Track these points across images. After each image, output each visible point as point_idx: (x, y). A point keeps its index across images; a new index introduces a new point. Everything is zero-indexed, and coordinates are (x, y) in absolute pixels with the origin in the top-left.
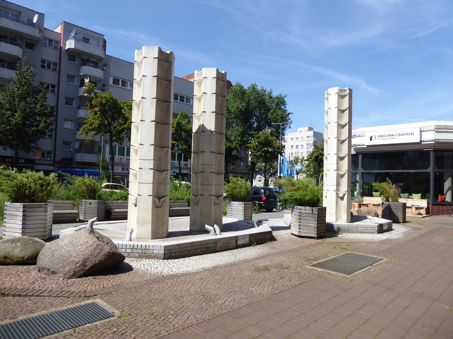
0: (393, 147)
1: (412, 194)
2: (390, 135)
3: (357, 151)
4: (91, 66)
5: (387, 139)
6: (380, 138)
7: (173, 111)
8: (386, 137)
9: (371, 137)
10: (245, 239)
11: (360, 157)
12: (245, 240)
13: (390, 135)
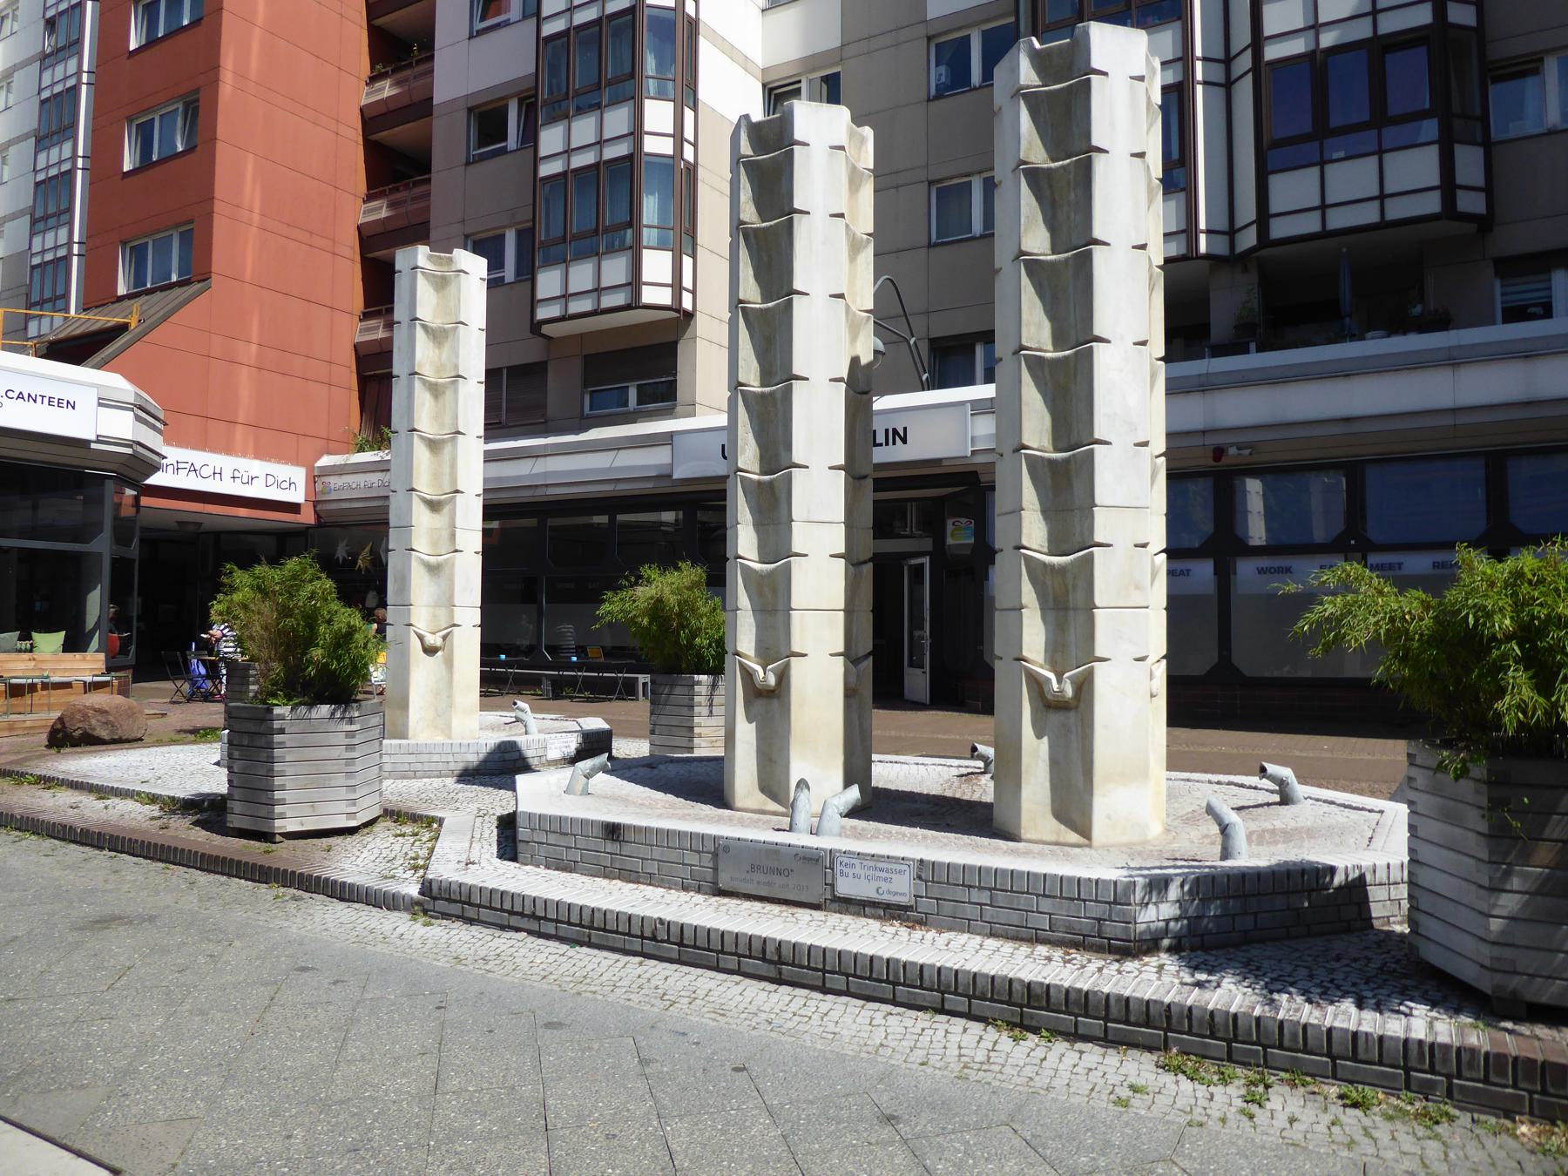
1: (1045, 739)
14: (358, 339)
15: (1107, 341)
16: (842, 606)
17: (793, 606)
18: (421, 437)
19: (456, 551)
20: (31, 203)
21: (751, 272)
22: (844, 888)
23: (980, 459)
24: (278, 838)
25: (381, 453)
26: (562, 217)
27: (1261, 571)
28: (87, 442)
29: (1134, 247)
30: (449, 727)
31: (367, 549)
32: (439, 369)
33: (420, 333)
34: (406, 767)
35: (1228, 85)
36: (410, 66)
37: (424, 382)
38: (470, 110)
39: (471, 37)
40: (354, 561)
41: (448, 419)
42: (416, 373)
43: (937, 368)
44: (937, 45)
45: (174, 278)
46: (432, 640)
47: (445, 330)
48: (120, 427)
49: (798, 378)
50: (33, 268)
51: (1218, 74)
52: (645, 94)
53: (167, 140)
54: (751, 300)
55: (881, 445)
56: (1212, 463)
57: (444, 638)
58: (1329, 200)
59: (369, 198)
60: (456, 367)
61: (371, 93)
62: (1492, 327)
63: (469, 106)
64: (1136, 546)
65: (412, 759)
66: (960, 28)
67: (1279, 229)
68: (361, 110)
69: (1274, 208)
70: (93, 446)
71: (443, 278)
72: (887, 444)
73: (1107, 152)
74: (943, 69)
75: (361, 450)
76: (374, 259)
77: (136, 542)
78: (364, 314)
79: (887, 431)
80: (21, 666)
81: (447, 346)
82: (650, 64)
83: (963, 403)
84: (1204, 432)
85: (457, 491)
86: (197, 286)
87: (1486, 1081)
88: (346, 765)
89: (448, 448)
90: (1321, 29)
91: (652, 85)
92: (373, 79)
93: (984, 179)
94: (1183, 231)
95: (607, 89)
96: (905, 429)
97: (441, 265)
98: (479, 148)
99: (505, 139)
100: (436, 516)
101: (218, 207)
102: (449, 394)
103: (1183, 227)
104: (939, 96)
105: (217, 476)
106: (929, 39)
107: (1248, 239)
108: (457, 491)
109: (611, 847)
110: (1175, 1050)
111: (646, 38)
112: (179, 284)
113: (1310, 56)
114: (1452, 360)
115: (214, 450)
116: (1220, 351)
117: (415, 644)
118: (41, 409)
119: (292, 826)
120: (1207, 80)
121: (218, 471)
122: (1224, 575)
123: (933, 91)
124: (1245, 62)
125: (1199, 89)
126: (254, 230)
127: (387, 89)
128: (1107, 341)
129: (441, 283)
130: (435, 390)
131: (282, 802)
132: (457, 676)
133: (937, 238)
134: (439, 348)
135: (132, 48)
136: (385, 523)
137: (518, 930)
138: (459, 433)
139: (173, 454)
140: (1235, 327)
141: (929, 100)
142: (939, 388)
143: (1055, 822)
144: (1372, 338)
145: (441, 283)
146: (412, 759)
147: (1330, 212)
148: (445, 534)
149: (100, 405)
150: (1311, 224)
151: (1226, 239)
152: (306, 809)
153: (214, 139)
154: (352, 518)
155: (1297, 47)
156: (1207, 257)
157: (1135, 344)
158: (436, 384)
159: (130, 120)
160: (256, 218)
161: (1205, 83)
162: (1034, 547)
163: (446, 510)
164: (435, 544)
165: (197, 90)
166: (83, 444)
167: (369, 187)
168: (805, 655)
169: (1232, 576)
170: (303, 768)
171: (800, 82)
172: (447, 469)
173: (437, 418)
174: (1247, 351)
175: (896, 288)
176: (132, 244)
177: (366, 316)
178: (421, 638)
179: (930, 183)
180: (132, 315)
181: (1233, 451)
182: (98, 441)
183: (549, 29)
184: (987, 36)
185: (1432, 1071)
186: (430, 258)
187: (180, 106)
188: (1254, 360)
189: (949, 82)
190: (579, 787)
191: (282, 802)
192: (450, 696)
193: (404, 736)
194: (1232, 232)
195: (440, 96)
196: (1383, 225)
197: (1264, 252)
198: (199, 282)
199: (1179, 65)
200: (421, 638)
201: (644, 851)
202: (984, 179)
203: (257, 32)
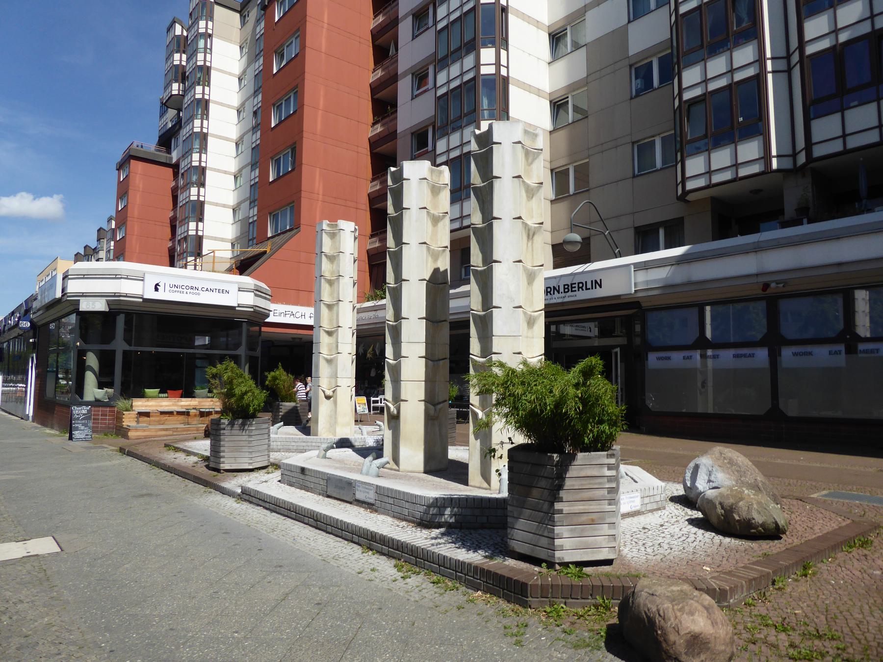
0: (198, 309)
1: (479, 440)
2: (192, 288)
3: (112, 307)
4: (630, 264)
5: (187, 293)
6: (173, 289)
7: (549, 270)
8: (185, 290)
9: (157, 285)
10: (633, 502)
11: (121, 320)
12: (633, 504)
13: (192, 288)
14: (369, 247)
15: (500, 262)
16: (424, 379)
17: (402, 379)
18: (324, 304)
19: (339, 353)
20: (249, 195)
21: (392, 235)
22: (360, 496)
23: (640, 295)
24: (222, 471)
25: (375, 302)
26: (459, 181)
27: (795, 354)
28: (234, 307)
29: (514, 219)
30: (335, 432)
31: (372, 347)
32: (332, 273)
33: (324, 258)
34: (302, 448)
35: (789, 71)
36: (388, 116)
37: (326, 279)
38: (412, 134)
39: (412, 99)
40: (366, 355)
41: (335, 295)
42: (322, 276)
43: (640, 243)
44: (636, 68)
45: (288, 228)
46: (329, 393)
47: (334, 256)
48: (248, 300)
49: (405, 280)
50: (250, 223)
51: (782, 65)
52: (481, 118)
53: (285, 166)
54: (392, 247)
55: (589, 289)
56: (760, 292)
57: (334, 392)
58: (847, 132)
59: (373, 180)
60: (339, 271)
61: (374, 130)
62: (800, 227)
63: (412, 131)
64: (514, 353)
65: (304, 444)
66: (646, 58)
67: (819, 151)
68: (369, 139)
69: (815, 139)
70: (237, 309)
71: (333, 233)
72: (592, 288)
73: (500, 178)
74: (639, 81)
75: (368, 301)
76: (377, 209)
77: (259, 349)
78: (371, 235)
79: (592, 281)
80: (208, 404)
81: (335, 263)
82: (485, 103)
83: (628, 265)
84: (757, 275)
85: (339, 327)
86: (295, 231)
87: (473, 577)
88: (249, 443)
89: (335, 308)
90: (840, 32)
91: (486, 113)
92: (374, 124)
93: (662, 138)
94: (762, 158)
95: (465, 118)
96: (601, 280)
97: (333, 228)
98: (418, 150)
99: (427, 146)
100: (330, 338)
101: (303, 194)
102: (336, 284)
103: (762, 155)
104: (637, 95)
105: (303, 317)
106: (631, 66)
107: (802, 159)
108: (339, 327)
109: (302, 477)
110: (402, 560)
111: (481, 90)
112: (290, 230)
113: (833, 49)
114: (757, 248)
115: (302, 305)
116: (785, 225)
117: (322, 395)
118: (216, 294)
119: (227, 467)
120: (774, 70)
121: (303, 314)
122: (774, 357)
123: (634, 93)
124: (796, 58)
125: (770, 77)
126: (320, 202)
127: (379, 129)
128: (500, 262)
129: (333, 235)
130: (330, 283)
131: (223, 457)
132: (339, 409)
133: (638, 172)
134: (332, 264)
135: (272, 126)
136: (312, 343)
137: (261, 506)
138: (340, 301)
139: (272, 306)
140: (795, 210)
141: (631, 98)
142: (642, 253)
143: (481, 478)
144: (878, 211)
145: (333, 235)
146: (304, 444)
147: (848, 139)
148: (334, 346)
149: (239, 290)
150: (837, 147)
151: (791, 159)
152: (232, 460)
153: (301, 164)
154: (366, 334)
155: (825, 44)
156: (778, 171)
157: (514, 262)
158: (330, 280)
159: (272, 158)
160: (321, 196)
161: (773, 72)
162: (475, 354)
163: (335, 335)
164: (330, 350)
165: (295, 143)
166: (233, 308)
167: (373, 175)
168: (407, 401)
169: (778, 358)
170: (231, 444)
171: (568, 97)
172: (335, 317)
173: (331, 294)
174: (802, 224)
175: (596, 208)
176: (274, 213)
177: (372, 236)
178: (324, 392)
179: (633, 143)
180: (267, 247)
181: (773, 285)
182: (239, 306)
183: (440, 92)
184: (661, 60)
185: (461, 573)
186: (328, 225)
187: (290, 150)
188: (807, 229)
189: (643, 87)
190: (321, 455)
191: (223, 457)
192: (336, 418)
193: (316, 435)
194: (794, 155)
195: (400, 129)
196: (846, 152)
197: (812, 165)
198: (296, 229)
199: (757, 64)
200: (324, 392)
201: (313, 479)
202: (662, 138)
203: (320, 112)
